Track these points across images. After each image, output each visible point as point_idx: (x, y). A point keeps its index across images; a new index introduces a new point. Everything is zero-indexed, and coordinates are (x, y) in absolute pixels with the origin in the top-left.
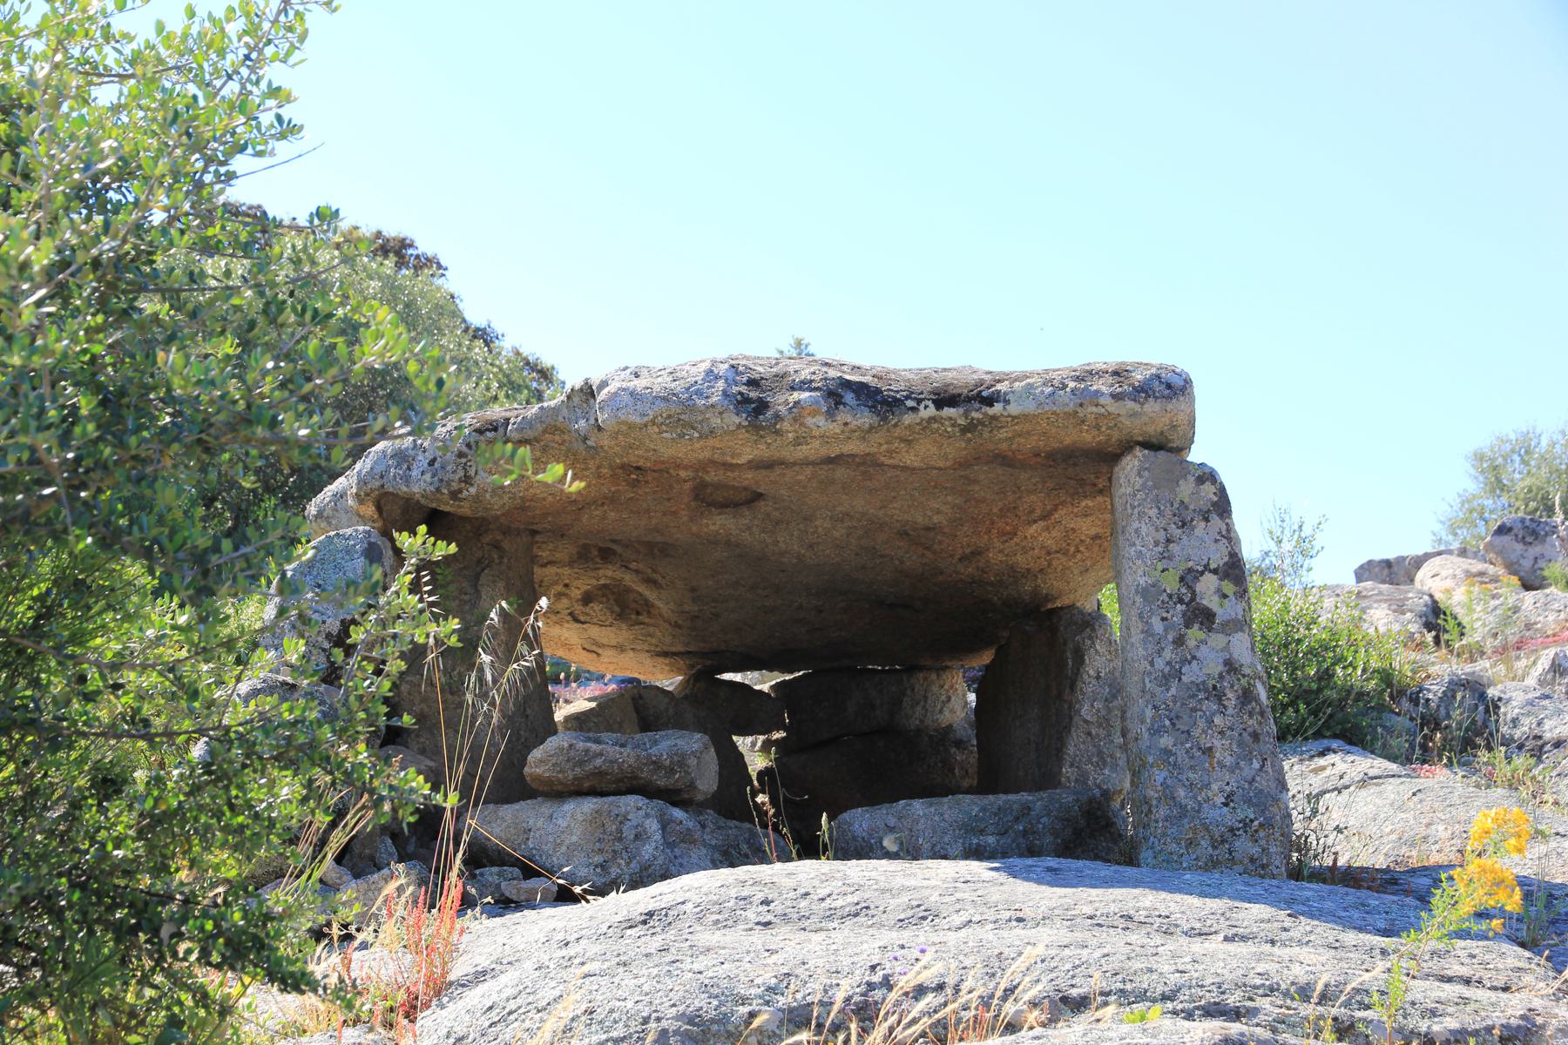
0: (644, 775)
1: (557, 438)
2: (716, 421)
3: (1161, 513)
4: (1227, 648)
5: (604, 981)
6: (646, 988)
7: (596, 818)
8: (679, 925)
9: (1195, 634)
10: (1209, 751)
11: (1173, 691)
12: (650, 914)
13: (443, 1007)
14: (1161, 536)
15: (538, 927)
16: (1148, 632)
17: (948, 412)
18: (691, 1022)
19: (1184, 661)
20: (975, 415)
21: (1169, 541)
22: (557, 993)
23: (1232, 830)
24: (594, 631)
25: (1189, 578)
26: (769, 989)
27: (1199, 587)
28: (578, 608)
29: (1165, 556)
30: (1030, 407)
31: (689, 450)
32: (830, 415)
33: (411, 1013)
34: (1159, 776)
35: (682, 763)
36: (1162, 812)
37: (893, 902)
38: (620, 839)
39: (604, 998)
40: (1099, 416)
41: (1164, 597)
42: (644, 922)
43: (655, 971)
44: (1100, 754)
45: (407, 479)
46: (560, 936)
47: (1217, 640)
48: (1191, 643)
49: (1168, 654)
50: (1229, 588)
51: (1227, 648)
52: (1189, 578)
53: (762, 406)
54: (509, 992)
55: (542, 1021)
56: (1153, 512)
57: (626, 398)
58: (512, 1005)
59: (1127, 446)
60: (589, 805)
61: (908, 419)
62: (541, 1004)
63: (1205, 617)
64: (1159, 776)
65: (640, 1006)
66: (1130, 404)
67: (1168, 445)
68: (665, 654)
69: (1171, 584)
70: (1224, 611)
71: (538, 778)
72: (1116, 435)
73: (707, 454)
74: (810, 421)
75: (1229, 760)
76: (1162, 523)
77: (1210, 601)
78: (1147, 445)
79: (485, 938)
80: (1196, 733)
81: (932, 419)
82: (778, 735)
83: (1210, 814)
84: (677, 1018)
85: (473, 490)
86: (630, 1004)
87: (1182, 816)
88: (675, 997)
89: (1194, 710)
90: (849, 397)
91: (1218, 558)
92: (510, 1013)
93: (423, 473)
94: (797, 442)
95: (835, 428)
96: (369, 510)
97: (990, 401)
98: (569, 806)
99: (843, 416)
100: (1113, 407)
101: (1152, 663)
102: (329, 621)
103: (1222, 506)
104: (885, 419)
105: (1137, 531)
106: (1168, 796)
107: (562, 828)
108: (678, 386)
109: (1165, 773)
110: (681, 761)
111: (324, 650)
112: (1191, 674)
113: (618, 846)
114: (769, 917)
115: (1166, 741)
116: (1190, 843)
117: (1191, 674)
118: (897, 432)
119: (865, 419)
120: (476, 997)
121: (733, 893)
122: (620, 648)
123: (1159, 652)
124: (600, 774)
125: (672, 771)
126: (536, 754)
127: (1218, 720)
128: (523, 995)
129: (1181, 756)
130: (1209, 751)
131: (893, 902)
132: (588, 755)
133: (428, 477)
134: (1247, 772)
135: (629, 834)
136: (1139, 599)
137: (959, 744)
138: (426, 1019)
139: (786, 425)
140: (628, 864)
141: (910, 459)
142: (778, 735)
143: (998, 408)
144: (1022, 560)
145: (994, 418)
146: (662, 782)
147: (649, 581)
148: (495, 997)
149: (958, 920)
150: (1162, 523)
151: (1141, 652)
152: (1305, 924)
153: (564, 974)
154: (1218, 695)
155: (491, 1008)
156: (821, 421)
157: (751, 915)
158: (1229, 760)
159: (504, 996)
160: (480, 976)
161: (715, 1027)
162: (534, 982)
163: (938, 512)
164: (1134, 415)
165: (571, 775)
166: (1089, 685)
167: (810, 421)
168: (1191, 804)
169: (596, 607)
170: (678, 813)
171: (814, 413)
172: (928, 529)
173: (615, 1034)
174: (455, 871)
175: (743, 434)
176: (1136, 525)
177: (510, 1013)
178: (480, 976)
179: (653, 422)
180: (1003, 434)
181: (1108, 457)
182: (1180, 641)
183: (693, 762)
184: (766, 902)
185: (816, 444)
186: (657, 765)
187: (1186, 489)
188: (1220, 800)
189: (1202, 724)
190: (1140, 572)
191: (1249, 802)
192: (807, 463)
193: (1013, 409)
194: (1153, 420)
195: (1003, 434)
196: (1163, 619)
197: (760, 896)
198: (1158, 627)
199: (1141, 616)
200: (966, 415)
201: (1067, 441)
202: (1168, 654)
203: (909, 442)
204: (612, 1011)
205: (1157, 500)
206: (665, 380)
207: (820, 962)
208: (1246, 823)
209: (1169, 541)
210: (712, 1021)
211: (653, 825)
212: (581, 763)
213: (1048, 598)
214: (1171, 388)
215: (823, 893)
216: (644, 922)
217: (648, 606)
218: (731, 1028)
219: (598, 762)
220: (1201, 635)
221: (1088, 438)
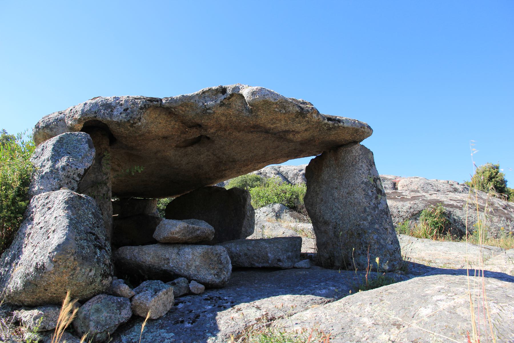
1: (184, 109)
7: (205, 255)
10: (386, 229)
11: (377, 212)
16: (367, 195)
20: (336, 125)
23: (394, 251)
30: (349, 125)
36: (376, 246)
38: (221, 263)
41: (371, 185)
44: (250, 224)
45: (111, 115)
48: (379, 199)
49: (374, 201)
56: (365, 161)
76: (367, 164)
80: (383, 224)
83: (389, 247)
85: (140, 124)
87: (383, 247)
89: (382, 217)
93: (121, 114)
97: (339, 121)
101: (369, 204)
102: (80, 169)
105: (361, 166)
106: (378, 242)
109: (377, 235)
111: (77, 181)
113: (221, 266)
115: (377, 226)
116: (385, 255)
124: (197, 237)
132: (195, 230)
133: (124, 115)
140: (227, 273)
145: (339, 127)
150: (367, 164)
176: (361, 164)
179: (276, 103)
182: (377, 198)
188: (390, 243)
189: (384, 221)
190: (364, 178)
196: (372, 191)
202: (374, 201)
209: (369, 170)
219: (198, 232)
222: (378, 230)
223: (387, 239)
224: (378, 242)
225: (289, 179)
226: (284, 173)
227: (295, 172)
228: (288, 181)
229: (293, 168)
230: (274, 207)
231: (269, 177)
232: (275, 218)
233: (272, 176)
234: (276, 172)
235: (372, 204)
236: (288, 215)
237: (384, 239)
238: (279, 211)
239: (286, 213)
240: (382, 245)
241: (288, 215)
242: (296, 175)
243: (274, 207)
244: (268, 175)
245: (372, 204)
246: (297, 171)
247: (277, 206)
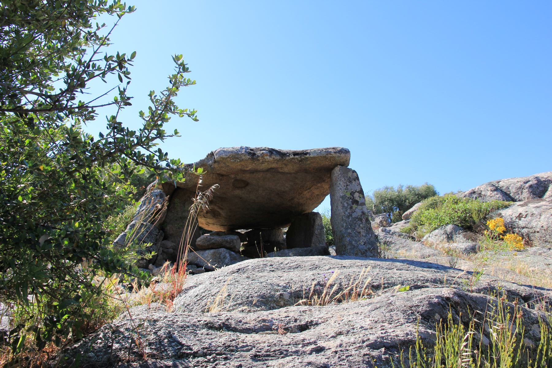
0: (224, 244)
2: (244, 157)
3: (345, 179)
4: (362, 209)
5: (232, 286)
6: (246, 288)
7: (213, 254)
8: (248, 272)
9: (354, 206)
10: (360, 233)
12: (239, 269)
13: (181, 296)
14: (345, 184)
15: (205, 276)
16: (343, 206)
17: (297, 157)
18: (262, 298)
19: (352, 212)
21: (347, 186)
22: (218, 290)
23: (366, 250)
24: (208, 220)
25: (352, 194)
26: (284, 287)
27: (355, 196)
28: (205, 215)
29: (347, 189)
30: (315, 155)
31: (237, 166)
32: (270, 156)
33: (172, 297)
34: (348, 239)
35: (232, 241)
36: (349, 247)
37: (307, 264)
39: (234, 292)
40: (331, 157)
42: (237, 272)
43: (247, 283)
46: (213, 276)
47: (360, 207)
48: (354, 208)
50: (361, 196)
51: (362, 209)
52: (352, 194)
53: (254, 154)
54: (202, 291)
55: (214, 299)
56: (343, 179)
57: (222, 152)
58: (203, 294)
59: (336, 165)
60: (212, 251)
61: (287, 158)
62: (213, 294)
63: (356, 202)
64: (348, 239)
65: (245, 293)
66: (338, 154)
67: (344, 164)
68: (223, 225)
69: (348, 195)
70: (360, 201)
71: (199, 245)
72: (334, 162)
73: (239, 167)
74: (265, 157)
75: (364, 235)
76: (345, 181)
77: (358, 199)
78: (340, 165)
79: (190, 280)
80: (356, 228)
81: (293, 158)
82: (245, 243)
83: (360, 247)
84: (258, 296)
86: (242, 293)
88: (256, 290)
90: (274, 152)
91: (358, 190)
92: (203, 297)
94: (263, 163)
95: (271, 159)
96: (161, 187)
97: (306, 154)
98: (207, 251)
99: (273, 156)
100: (334, 155)
103: (357, 178)
104: (282, 158)
106: (350, 243)
107: (205, 257)
108: (234, 150)
110: (232, 241)
112: (354, 215)
113: (220, 260)
114: (273, 269)
115: (349, 231)
117: (354, 215)
118: (285, 162)
119: (278, 157)
120: (192, 292)
121: (261, 263)
122: (213, 224)
123: (346, 211)
124: (213, 244)
125: (230, 243)
126: (199, 239)
127: (361, 225)
128: (207, 291)
129: (353, 234)
130: (360, 233)
131: (307, 264)
134: (368, 237)
135: (222, 257)
136: (341, 199)
137: (282, 244)
138: (176, 300)
139: (260, 158)
141: (286, 170)
142: (245, 243)
143: (308, 156)
144: (301, 201)
145: (307, 158)
146: (228, 246)
147: (220, 208)
148: (198, 292)
149: (327, 267)
150: (345, 181)
151: (342, 211)
152: (417, 268)
153: (219, 285)
154: (361, 220)
155: (197, 296)
156: (268, 157)
157: (268, 268)
158: (364, 235)
159: (201, 292)
160: (191, 288)
161: (270, 299)
162: (210, 287)
163: (287, 187)
164: (339, 157)
165: (206, 244)
166: (317, 227)
167: (265, 157)
168: (356, 245)
169: (209, 215)
170: (232, 253)
171: (267, 155)
172: (284, 192)
173: (239, 302)
174: (186, 254)
175: (250, 161)
177: (203, 297)
178: (191, 288)
179: (229, 157)
180: (308, 162)
181: (329, 170)
182: (351, 208)
183: (235, 241)
184: (271, 265)
185: (266, 164)
186: (227, 242)
187: (350, 174)
188: (363, 244)
189: (357, 226)
191: (369, 244)
192: (263, 171)
193: (311, 156)
194: (343, 158)
195: (308, 162)
197: (269, 264)
198: (346, 205)
199: (341, 203)
200: (301, 157)
201: (322, 164)
202: (349, 211)
203: (286, 165)
204: (236, 295)
205: (344, 177)
206: (232, 149)
207: (297, 279)
208: (369, 249)
209: (347, 186)
210: (269, 297)
211: (228, 255)
212: (209, 241)
213: (304, 211)
214: (346, 152)
215: (286, 262)
216: (237, 272)
217: (219, 214)
218: (275, 299)
219: (213, 241)
220: (356, 206)
221: (327, 163)
222: (350, 233)
223: (360, 241)
224: (350, 243)
225: (511, 195)
226: (504, 189)
227: (519, 185)
228: (510, 197)
229: (516, 181)
230: (446, 229)
231: (485, 195)
232: (445, 240)
233: (489, 193)
234: (494, 188)
235: (347, 213)
236: (461, 236)
237: (356, 241)
238: (451, 233)
239: (459, 234)
240: (354, 246)
241: (461, 236)
242: (521, 188)
243: (446, 229)
244: (483, 193)
245: (347, 213)
246: (522, 183)
247: (449, 228)
